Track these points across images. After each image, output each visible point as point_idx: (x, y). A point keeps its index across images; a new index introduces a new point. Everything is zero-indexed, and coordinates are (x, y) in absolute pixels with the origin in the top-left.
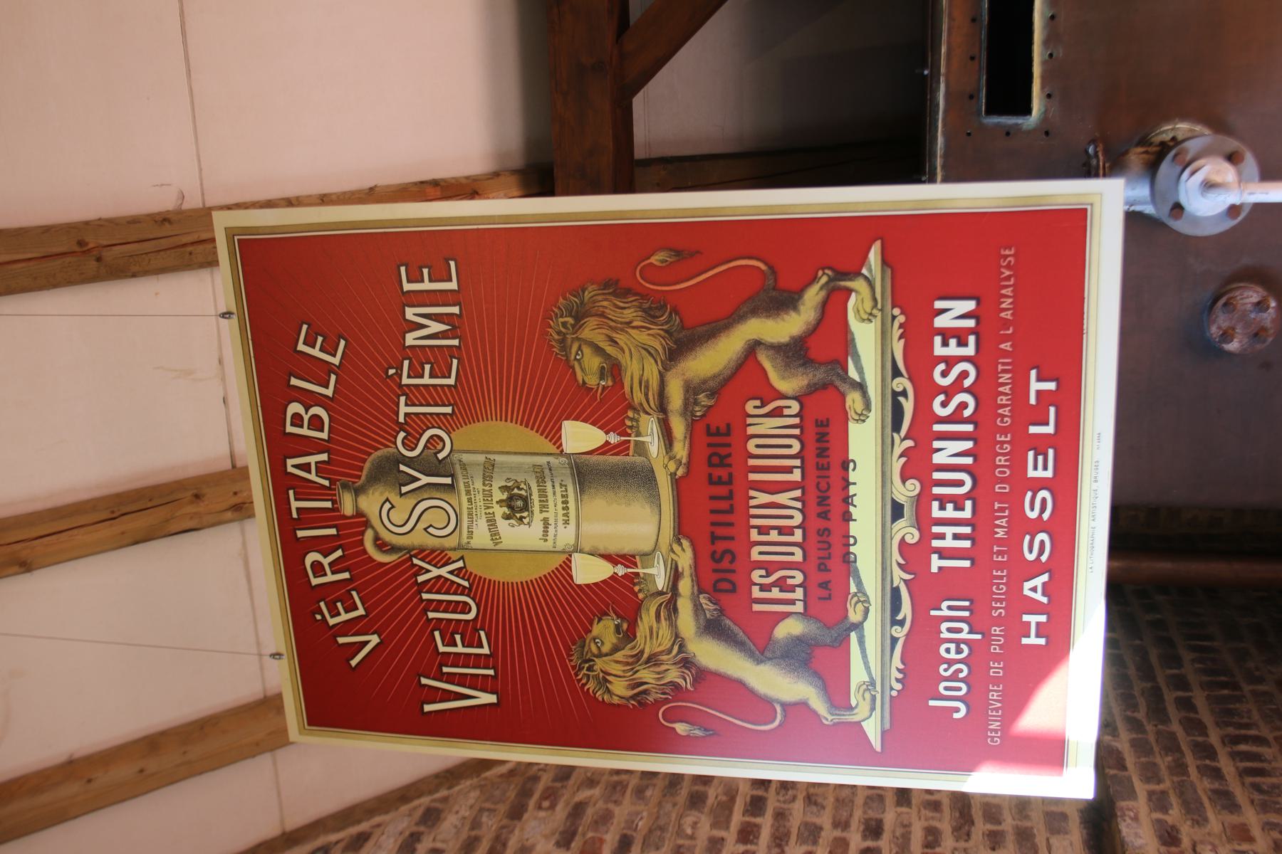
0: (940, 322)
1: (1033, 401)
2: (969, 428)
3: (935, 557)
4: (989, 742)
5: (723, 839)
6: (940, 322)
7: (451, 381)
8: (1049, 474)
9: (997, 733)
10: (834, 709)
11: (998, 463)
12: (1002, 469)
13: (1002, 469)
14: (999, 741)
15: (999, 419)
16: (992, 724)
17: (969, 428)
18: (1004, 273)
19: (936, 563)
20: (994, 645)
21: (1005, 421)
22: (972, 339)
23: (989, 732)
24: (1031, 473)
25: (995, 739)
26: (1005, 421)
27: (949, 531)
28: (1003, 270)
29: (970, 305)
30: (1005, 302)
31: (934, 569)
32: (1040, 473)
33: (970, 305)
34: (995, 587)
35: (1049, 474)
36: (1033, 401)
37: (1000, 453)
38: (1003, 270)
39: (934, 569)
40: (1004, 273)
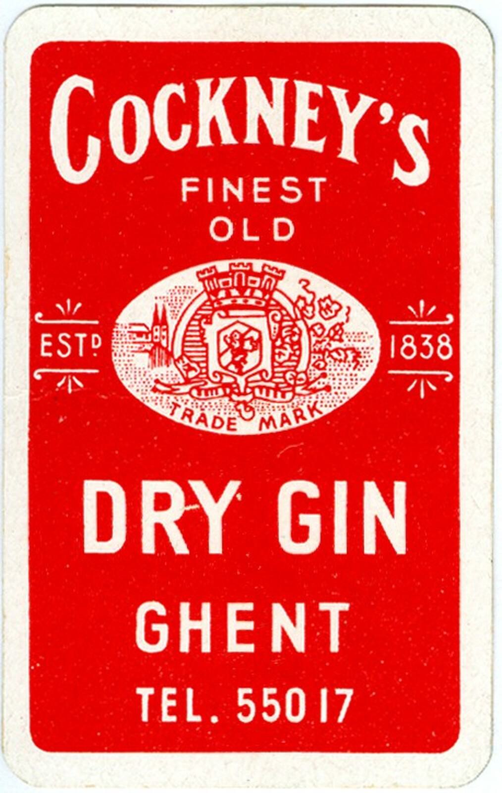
0: (278, 611)
1: (184, 199)
2: (341, 489)
3: (151, 691)
6: (278, 611)
8: (257, 199)
9: (313, 135)
17: (341, 489)
19: (145, 693)
22: (318, 146)
23: (173, 691)
24: (256, 180)
25: (312, 521)
27: (205, 625)
29: (400, 546)
31: (139, 691)
32: (256, 189)
33: (400, 546)
35: (257, 199)
36: (184, 199)
39: (139, 691)
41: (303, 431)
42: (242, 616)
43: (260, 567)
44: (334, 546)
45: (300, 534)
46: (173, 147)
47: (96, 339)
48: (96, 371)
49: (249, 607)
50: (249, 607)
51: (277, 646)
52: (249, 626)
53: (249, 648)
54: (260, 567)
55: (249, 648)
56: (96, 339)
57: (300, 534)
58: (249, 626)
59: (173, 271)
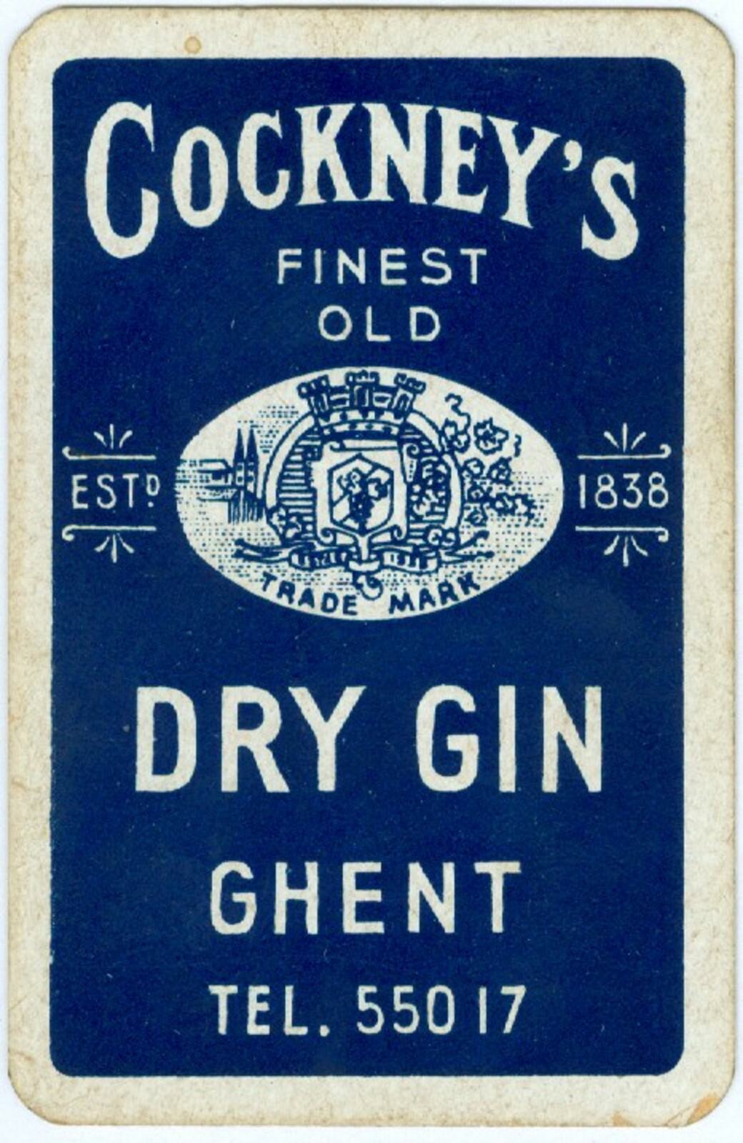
2: (507, 696)
4: (102, 505)
5: (424, 385)
7: (414, 337)
10: (468, 553)
11: (233, 697)
12: (430, 1017)
13: (430, 1017)
14: (425, 255)
15: (362, 1028)
16: (438, 886)
17: (507, 696)
18: (327, 707)
20: (590, 497)
21: (455, 742)
25: (465, 745)
26: (455, 742)
28: (543, 139)
30: (424, 905)
34: (397, 1027)
37: (258, 919)
38: (543, 139)
40: (327, 707)
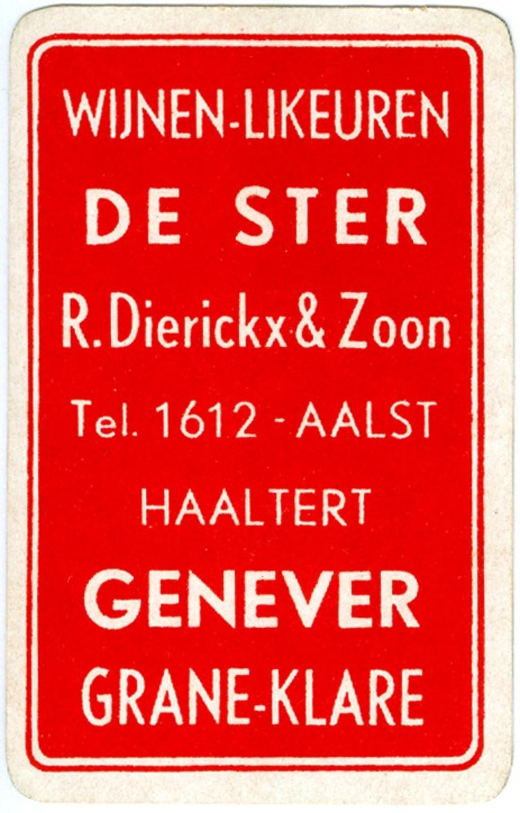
25: (106, 699)
41: (260, 716)
42: (166, 204)
43: (281, 420)
44: (188, 585)
45: (98, 710)
46: (507, 37)
47: (132, 681)
48: (248, 492)
49: (362, 193)
50: (362, 193)
51: (392, 238)
52: (361, 217)
53: (363, 239)
54: (281, 420)
55: (363, 239)
56: (132, 681)
57: (98, 710)
58: (361, 217)
59: (242, 499)
